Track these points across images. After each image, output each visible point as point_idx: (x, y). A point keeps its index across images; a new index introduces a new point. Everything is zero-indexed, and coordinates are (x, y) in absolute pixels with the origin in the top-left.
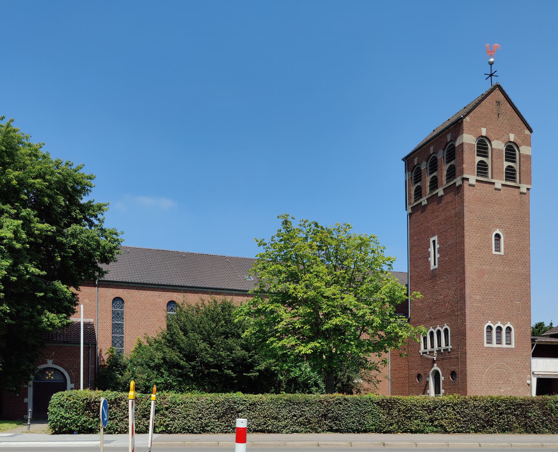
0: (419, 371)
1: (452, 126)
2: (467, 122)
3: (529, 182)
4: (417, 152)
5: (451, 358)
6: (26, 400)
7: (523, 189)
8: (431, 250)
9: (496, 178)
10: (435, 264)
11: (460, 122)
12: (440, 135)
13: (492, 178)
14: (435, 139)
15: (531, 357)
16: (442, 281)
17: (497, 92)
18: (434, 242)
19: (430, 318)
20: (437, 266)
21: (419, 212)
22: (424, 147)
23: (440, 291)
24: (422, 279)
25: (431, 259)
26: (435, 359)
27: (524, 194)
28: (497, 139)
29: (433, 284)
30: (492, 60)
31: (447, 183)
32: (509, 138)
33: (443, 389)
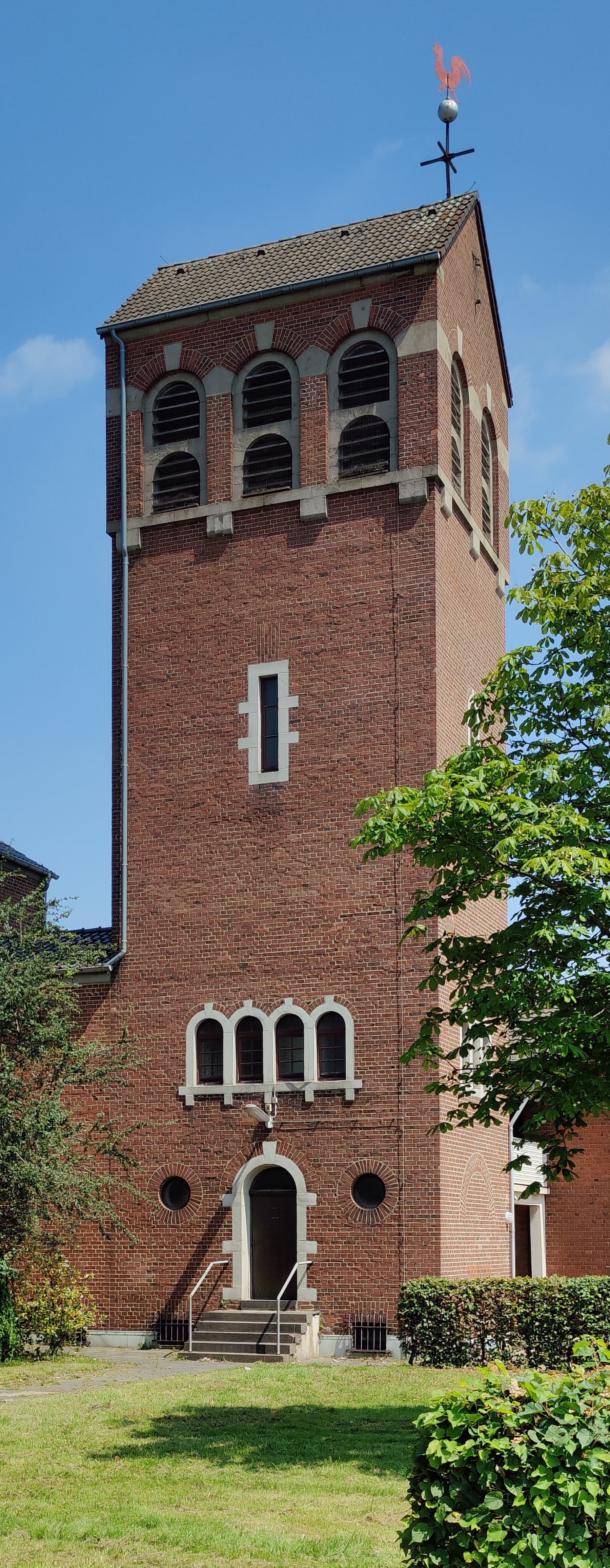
0: (174, 1167)
1: (382, 278)
4: (323, 292)
5: (354, 1126)
6: (242, 708)
11: (420, 271)
12: (314, 294)
14: (289, 300)
15: (512, 1133)
16: (314, 834)
19: (244, 966)
21: (188, 556)
22: (225, 314)
23: (300, 872)
24: (197, 812)
26: (270, 1125)
29: (260, 841)
30: (452, 104)
31: (158, 510)
33: (309, 1239)
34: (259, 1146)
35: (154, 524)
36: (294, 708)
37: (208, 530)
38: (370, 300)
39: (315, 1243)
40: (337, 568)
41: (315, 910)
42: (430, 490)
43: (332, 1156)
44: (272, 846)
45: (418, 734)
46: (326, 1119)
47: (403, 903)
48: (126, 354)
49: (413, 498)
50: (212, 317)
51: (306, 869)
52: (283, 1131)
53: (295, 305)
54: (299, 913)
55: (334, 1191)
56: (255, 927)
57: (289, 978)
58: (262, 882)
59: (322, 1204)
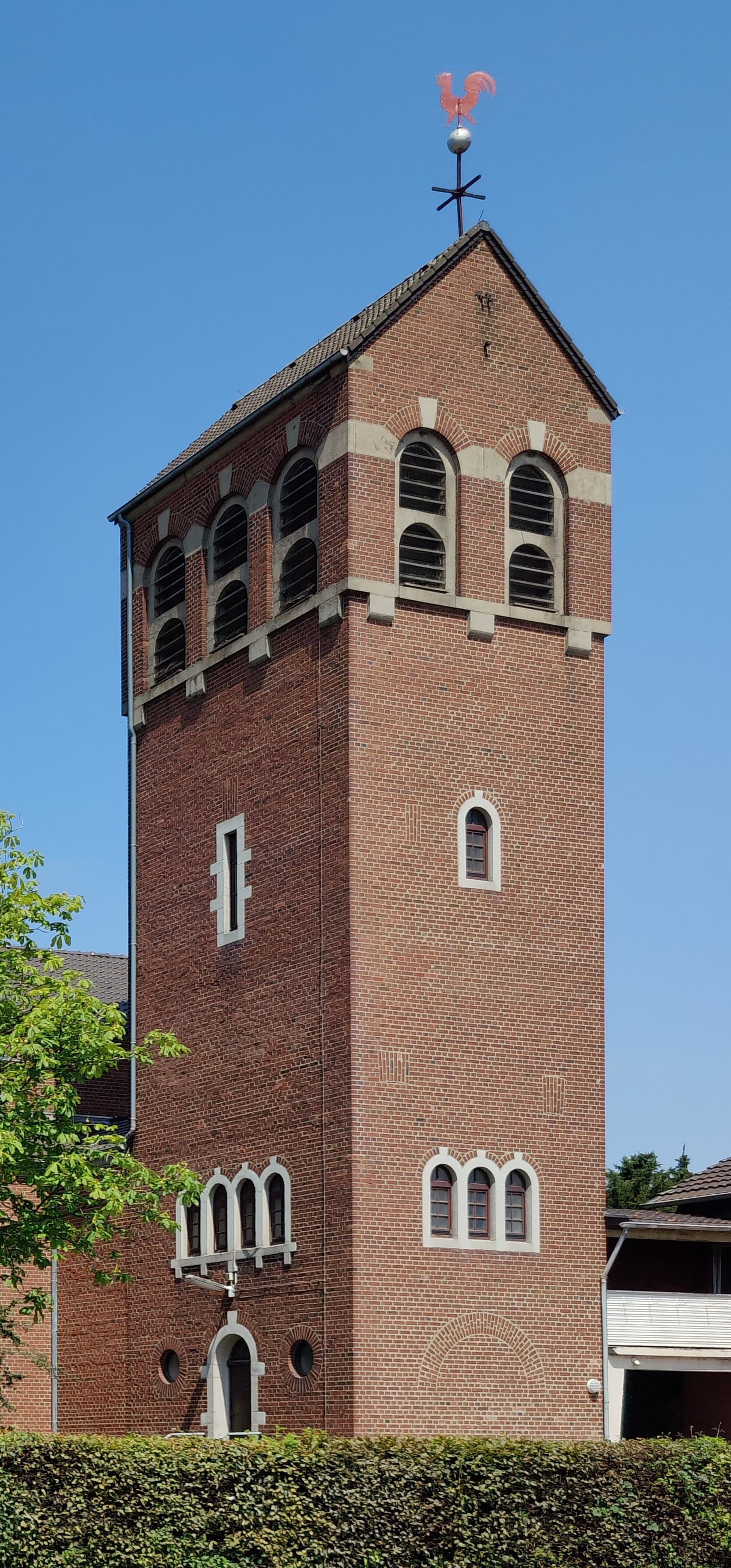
1: (306, 391)
2: (363, 374)
3: (604, 611)
5: (292, 1290)
7: (580, 639)
8: (221, 868)
9: (476, 595)
10: (234, 926)
11: (335, 372)
12: (258, 425)
13: (459, 593)
14: (240, 439)
16: (262, 990)
17: (482, 257)
18: (231, 837)
20: (240, 934)
21: (176, 724)
24: (184, 982)
25: (221, 905)
26: (231, 1294)
27: (584, 655)
28: (481, 442)
29: (226, 1004)
30: (462, 133)
32: (525, 439)
34: (225, 1316)
35: (152, 698)
36: (249, 862)
37: (187, 695)
38: (299, 417)
39: (264, 1413)
40: (278, 709)
41: (264, 1068)
42: (345, 606)
43: (276, 1323)
44: (234, 1007)
45: (336, 870)
46: (271, 1285)
47: (325, 1052)
48: (132, 534)
49: (330, 619)
50: (189, 476)
51: (256, 1027)
52: (241, 1299)
53: (245, 442)
54: (252, 1074)
55: (277, 1359)
56: (222, 1092)
57: (246, 1142)
58: (227, 1045)
59: (270, 1373)
